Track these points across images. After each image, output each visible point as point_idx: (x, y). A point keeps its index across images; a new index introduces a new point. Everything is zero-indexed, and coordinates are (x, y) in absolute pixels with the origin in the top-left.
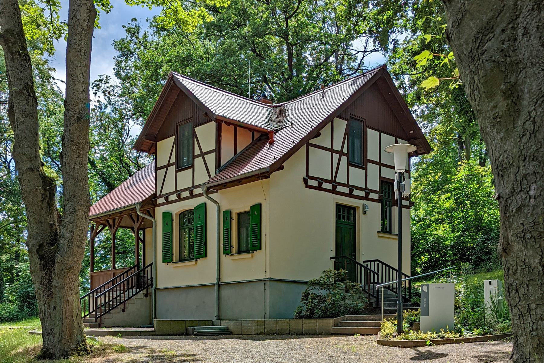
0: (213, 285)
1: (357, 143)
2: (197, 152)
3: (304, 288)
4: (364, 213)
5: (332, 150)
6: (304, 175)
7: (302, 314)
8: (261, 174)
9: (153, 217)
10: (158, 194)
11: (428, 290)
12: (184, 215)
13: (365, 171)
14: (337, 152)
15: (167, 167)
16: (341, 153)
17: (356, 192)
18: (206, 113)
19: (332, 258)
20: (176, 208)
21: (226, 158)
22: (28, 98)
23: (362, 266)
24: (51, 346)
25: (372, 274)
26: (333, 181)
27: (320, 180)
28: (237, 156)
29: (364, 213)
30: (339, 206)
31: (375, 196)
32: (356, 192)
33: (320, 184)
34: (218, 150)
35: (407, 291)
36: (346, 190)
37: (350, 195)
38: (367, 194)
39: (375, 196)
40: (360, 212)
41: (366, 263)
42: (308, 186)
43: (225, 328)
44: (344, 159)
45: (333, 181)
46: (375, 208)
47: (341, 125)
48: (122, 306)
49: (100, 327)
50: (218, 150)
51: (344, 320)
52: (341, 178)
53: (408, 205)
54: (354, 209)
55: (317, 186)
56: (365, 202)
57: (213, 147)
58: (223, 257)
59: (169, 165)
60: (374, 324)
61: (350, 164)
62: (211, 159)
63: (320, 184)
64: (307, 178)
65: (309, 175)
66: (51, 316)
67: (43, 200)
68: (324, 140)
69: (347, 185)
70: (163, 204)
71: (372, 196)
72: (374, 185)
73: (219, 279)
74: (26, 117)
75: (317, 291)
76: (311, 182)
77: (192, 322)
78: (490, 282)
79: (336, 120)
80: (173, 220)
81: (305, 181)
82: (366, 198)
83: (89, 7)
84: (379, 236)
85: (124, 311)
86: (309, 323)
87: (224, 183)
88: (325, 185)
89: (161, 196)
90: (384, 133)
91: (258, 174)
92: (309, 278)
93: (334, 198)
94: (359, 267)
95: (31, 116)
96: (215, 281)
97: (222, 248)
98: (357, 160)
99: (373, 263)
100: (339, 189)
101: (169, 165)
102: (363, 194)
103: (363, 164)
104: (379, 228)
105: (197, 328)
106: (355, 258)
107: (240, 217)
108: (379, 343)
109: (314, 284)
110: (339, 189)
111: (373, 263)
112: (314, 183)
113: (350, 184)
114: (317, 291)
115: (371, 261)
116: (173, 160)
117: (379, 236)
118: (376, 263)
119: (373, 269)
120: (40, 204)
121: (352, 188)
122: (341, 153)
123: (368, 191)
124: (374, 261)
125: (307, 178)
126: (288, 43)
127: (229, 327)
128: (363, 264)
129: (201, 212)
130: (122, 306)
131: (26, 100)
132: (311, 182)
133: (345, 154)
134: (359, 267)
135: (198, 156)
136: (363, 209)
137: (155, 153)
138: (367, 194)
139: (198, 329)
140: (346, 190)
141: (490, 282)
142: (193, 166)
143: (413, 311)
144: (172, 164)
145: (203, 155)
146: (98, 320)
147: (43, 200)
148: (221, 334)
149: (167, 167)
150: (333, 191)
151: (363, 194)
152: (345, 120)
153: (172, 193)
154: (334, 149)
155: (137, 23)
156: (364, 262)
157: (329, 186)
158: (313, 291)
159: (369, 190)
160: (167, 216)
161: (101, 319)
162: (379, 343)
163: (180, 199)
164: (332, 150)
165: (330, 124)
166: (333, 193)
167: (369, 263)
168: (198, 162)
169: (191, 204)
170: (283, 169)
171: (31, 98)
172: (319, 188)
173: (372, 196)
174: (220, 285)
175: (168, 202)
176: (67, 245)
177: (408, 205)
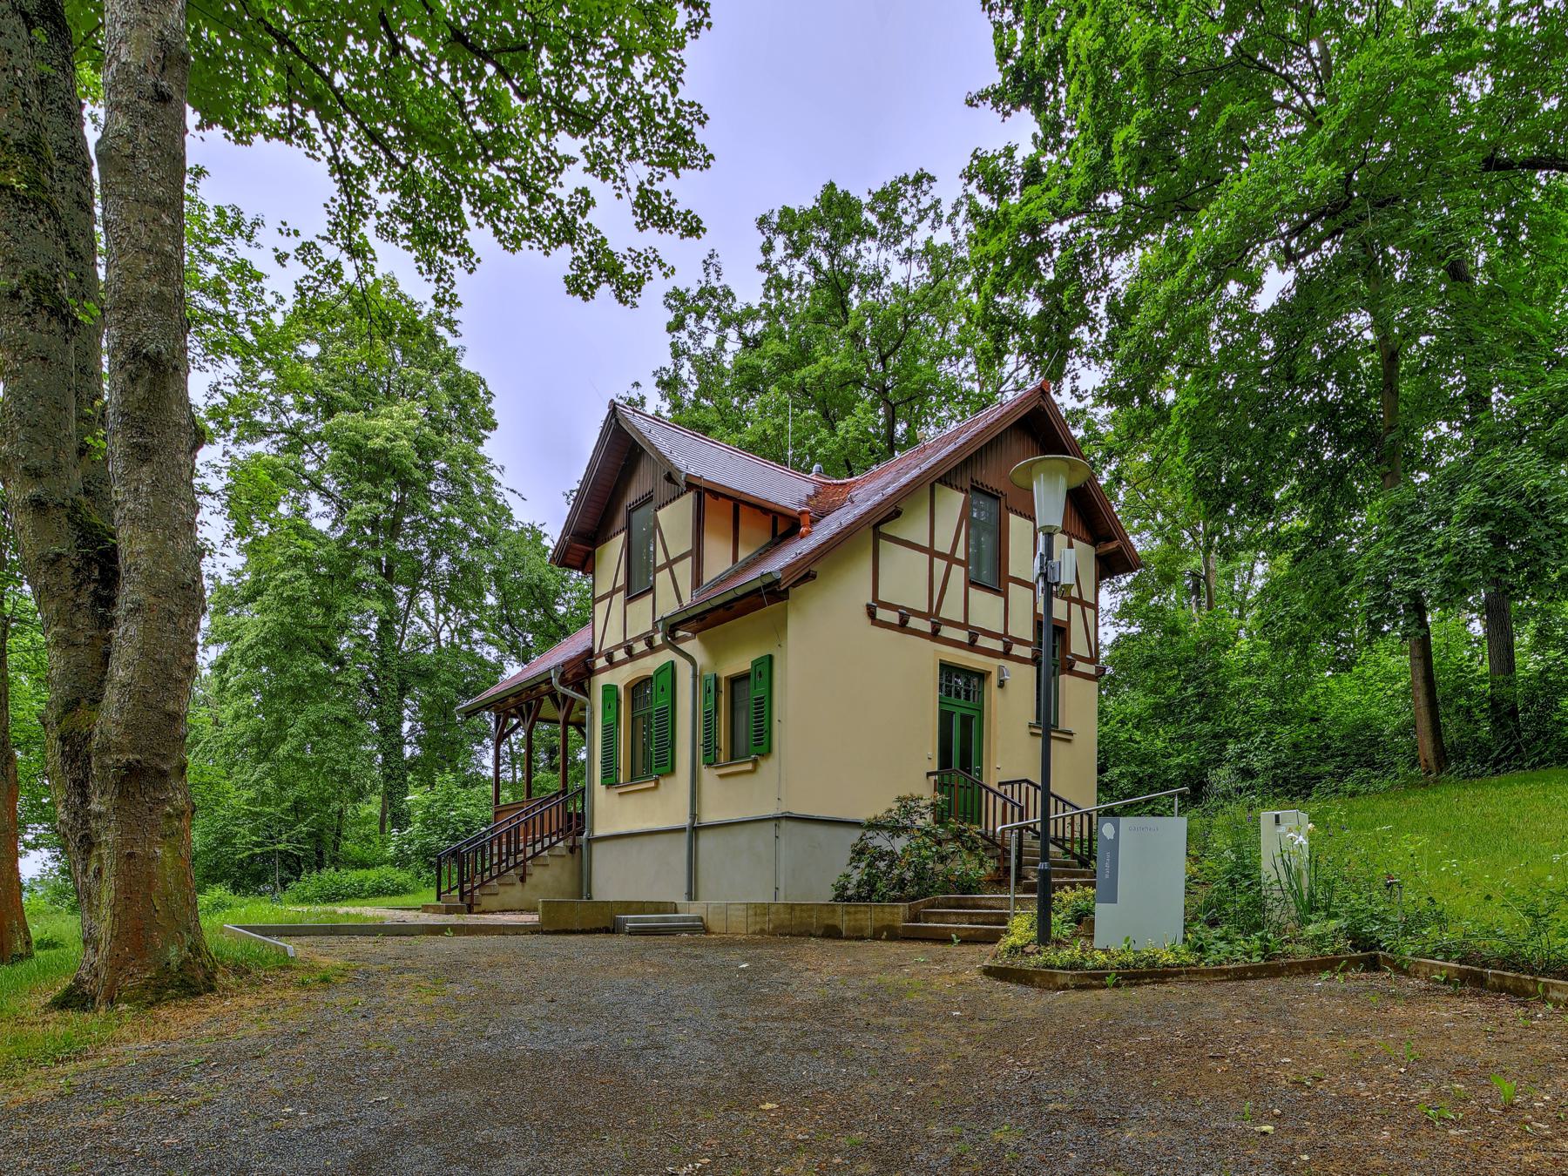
0: (681, 830)
1: (987, 541)
2: (661, 559)
3: (854, 835)
4: (1001, 685)
5: (932, 553)
7: (850, 893)
8: (765, 587)
9: (587, 694)
10: (597, 651)
11: (1117, 835)
12: (639, 688)
13: (1002, 599)
14: (942, 556)
15: (610, 595)
16: (950, 559)
17: (983, 642)
18: (669, 474)
20: (621, 677)
22: (34, 310)
23: (996, 794)
24: (87, 973)
25: (1009, 805)
26: (931, 615)
29: (1001, 685)
30: (947, 669)
31: (1026, 652)
32: (983, 642)
36: (962, 636)
37: (971, 646)
38: (1008, 648)
39: (1026, 652)
40: (994, 680)
41: (1003, 787)
43: (694, 919)
44: (958, 573)
45: (931, 615)
46: (1022, 678)
48: (520, 871)
49: (470, 912)
50: (697, 554)
51: (933, 907)
52: (952, 609)
53: (1093, 672)
54: (982, 676)
55: (897, 622)
56: (1001, 662)
57: (687, 545)
58: (708, 776)
59: (615, 591)
60: (994, 919)
61: (971, 583)
62: (684, 570)
66: (89, 895)
67: (80, 585)
68: (914, 528)
69: (964, 626)
70: (604, 670)
71: (1017, 650)
72: (1022, 627)
73: (694, 816)
74: (23, 361)
75: (881, 841)
76: (882, 614)
77: (628, 906)
78: (1277, 817)
80: (618, 700)
81: (871, 613)
82: (1006, 654)
83: (160, 32)
84: (1032, 734)
85: (523, 880)
86: (856, 913)
87: (699, 614)
88: (914, 622)
89: (600, 655)
91: (758, 590)
92: (864, 816)
93: (936, 651)
94: (991, 795)
95: (42, 358)
96: (685, 821)
97: (700, 751)
98: (986, 576)
99: (1016, 786)
100: (946, 632)
101: (615, 591)
102: (998, 646)
103: (997, 581)
105: (631, 920)
106: (980, 777)
107: (736, 687)
108: (988, 972)
109: (875, 826)
110: (946, 632)
111: (1016, 786)
112: (893, 617)
113: (971, 623)
114: (881, 841)
115: (1012, 783)
116: (621, 581)
117: (1032, 734)
118: (1024, 785)
119: (1016, 800)
120: (71, 594)
121: (975, 633)
122: (950, 559)
123: (1009, 641)
124: (1020, 782)
126: (887, 401)
127: (704, 917)
128: (996, 789)
129: (665, 680)
130: (520, 871)
131: (28, 315)
132: (882, 614)
133: (959, 562)
134: (991, 795)
135: (662, 568)
136: (999, 676)
137: (593, 572)
139: (635, 921)
140: (962, 636)
141: (1277, 817)
142: (652, 589)
143: (1087, 889)
144: (619, 590)
145: (670, 564)
146: (467, 900)
147: (80, 585)
148: (682, 931)
149: (610, 595)
150: (934, 635)
151: (998, 646)
152: (961, 490)
153: (618, 647)
155: (641, 391)
156: (1000, 784)
157: (925, 626)
158: (876, 842)
159: (1011, 637)
160: (609, 690)
161: (472, 896)
162: (988, 972)
163: (631, 656)
164: (932, 553)
167: (1009, 787)
168: (663, 578)
169: (649, 665)
171: (45, 312)
172: (902, 626)
173: (1017, 650)
174: (695, 830)
175: (612, 664)
176: (118, 700)
177: (1093, 672)
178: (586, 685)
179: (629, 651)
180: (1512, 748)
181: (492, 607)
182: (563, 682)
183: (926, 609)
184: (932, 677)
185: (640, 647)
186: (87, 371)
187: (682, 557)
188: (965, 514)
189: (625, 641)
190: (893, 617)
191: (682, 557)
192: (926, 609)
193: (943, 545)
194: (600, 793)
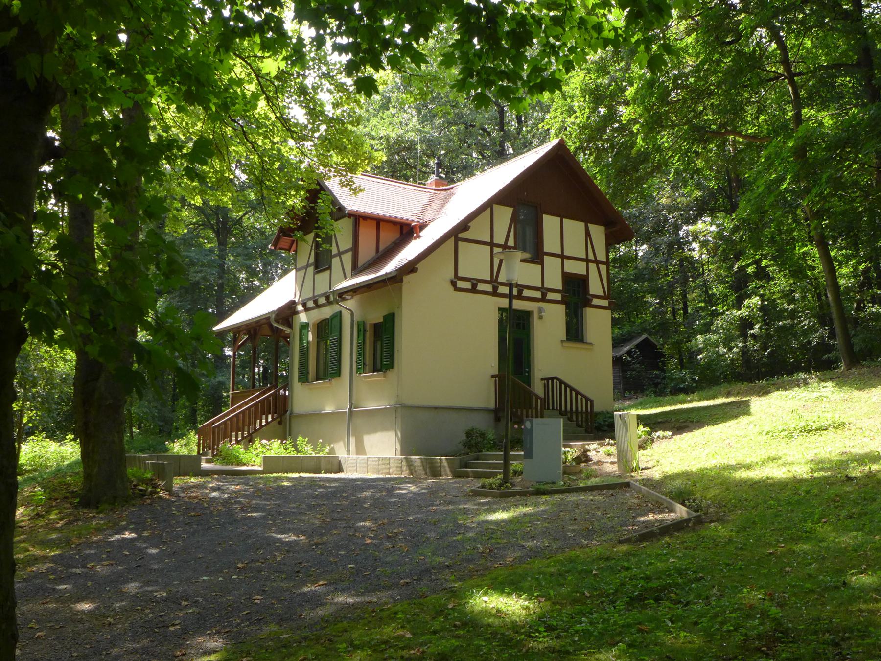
1: (529, 232)
5: (492, 245)
6: (451, 275)
13: (539, 267)
19: (493, 376)
21: (363, 258)
26: (494, 281)
27: (475, 282)
28: (379, 254)
29: (541, 318)
33: (474, 286)
34: (355, 249)
35: (584, 415)
38: (544, 295)
39: (558, 297)
42: (457, 289)
47: (505, 215)
50: (355, 249)
56: (541, 304)
57: (349, 245)
59: (307, 266)
62: (348, 258)
63: (474, 286)
64: (455, 280)
65: (459, 275)
71: (551, 296)
72: (555, 281)
76: (461, 284)
79: (496, 207)
81: (453, 284)
82: (543, 299)
90: (567, 218)
97: (355, 365)
99: (550, 381)
101: (307, 266)
102: (538, 294)
104: (562, 333)
111: (550, 381)
116: (312, 260)
123: (544, 291)
124: (553, 379)
125: (455, 280)
129: (336, 322)
132: (461, 284)
135: (335, 256)
138: (544, 295)
142: (330, 268)
144: (311, 265)
145: (340, 254)
150: (495, 293)
151: (538, 294)
153: (309, 299)
154: (495, 242)
157: (489, 288)
164: (492, 245)
165: (489, 210)
166: (493, 296)
168: (335, 261)
170: (416, 271)
172: (474, 290)
173: (551, 296)
178: (290, 320)
179: (316, 302)
180: (574, 418)
181: (147, 73)
182: (277, 321)
183: (489, 279)
184: (495, 317)
185: (322, 301)
186: (364, 521)
187: (346, 251)
188: (514, 219)
189: (314, 296)
190: (467, 285)
191: (346, 251)
192: (489, 279)
193: (499, 239)
194: (297, 385)
